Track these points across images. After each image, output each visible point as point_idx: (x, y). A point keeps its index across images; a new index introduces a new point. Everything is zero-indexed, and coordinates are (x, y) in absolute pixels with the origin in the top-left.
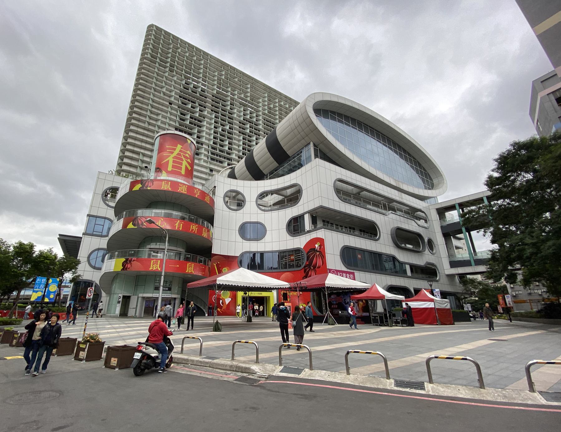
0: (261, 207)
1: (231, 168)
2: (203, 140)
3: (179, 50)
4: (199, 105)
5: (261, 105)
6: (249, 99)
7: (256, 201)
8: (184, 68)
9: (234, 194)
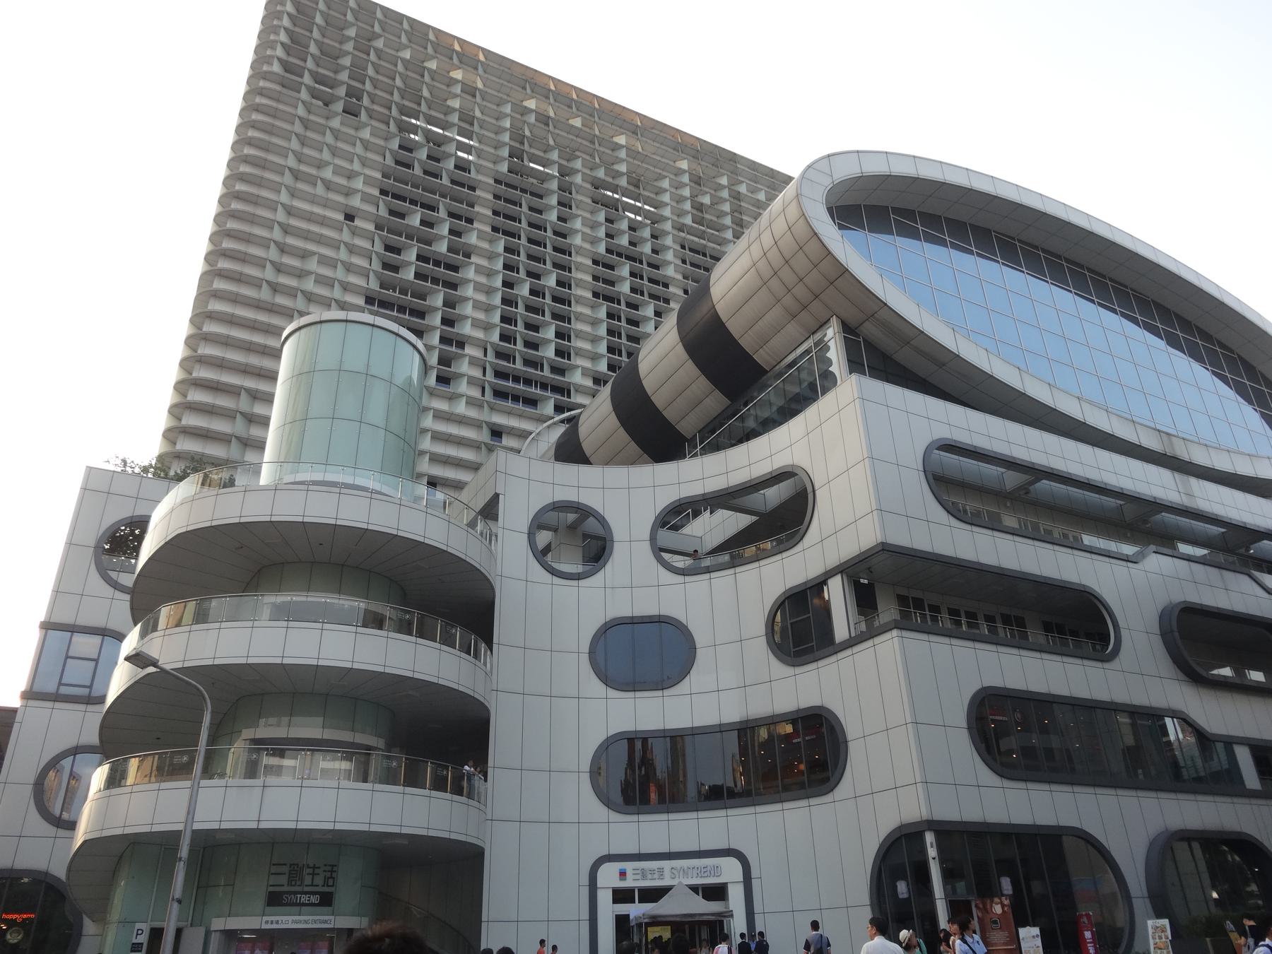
0: (666, 556)
1: (569, 420)
2: (466, 329)
3: (379, 43)
4: (451, 215)
5: (666, 198)
6: (623, 182)
7: (653, 539)
8: (396, 97)
9: (571, 517)
